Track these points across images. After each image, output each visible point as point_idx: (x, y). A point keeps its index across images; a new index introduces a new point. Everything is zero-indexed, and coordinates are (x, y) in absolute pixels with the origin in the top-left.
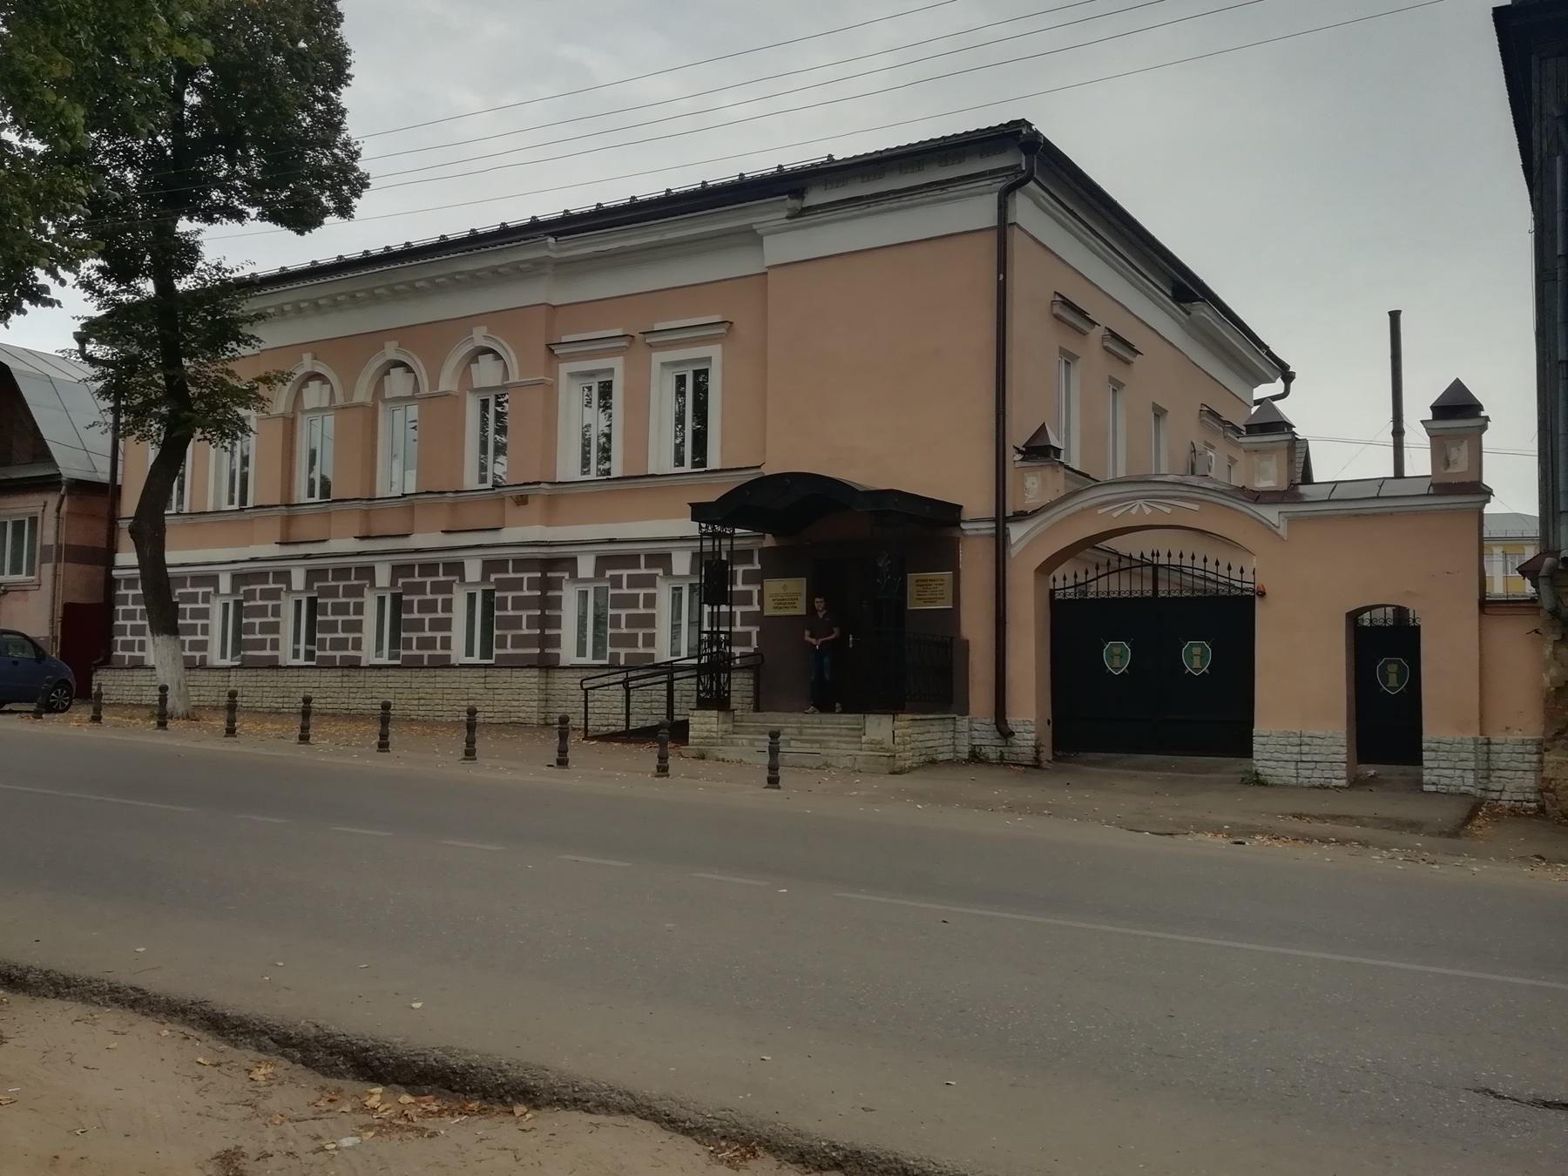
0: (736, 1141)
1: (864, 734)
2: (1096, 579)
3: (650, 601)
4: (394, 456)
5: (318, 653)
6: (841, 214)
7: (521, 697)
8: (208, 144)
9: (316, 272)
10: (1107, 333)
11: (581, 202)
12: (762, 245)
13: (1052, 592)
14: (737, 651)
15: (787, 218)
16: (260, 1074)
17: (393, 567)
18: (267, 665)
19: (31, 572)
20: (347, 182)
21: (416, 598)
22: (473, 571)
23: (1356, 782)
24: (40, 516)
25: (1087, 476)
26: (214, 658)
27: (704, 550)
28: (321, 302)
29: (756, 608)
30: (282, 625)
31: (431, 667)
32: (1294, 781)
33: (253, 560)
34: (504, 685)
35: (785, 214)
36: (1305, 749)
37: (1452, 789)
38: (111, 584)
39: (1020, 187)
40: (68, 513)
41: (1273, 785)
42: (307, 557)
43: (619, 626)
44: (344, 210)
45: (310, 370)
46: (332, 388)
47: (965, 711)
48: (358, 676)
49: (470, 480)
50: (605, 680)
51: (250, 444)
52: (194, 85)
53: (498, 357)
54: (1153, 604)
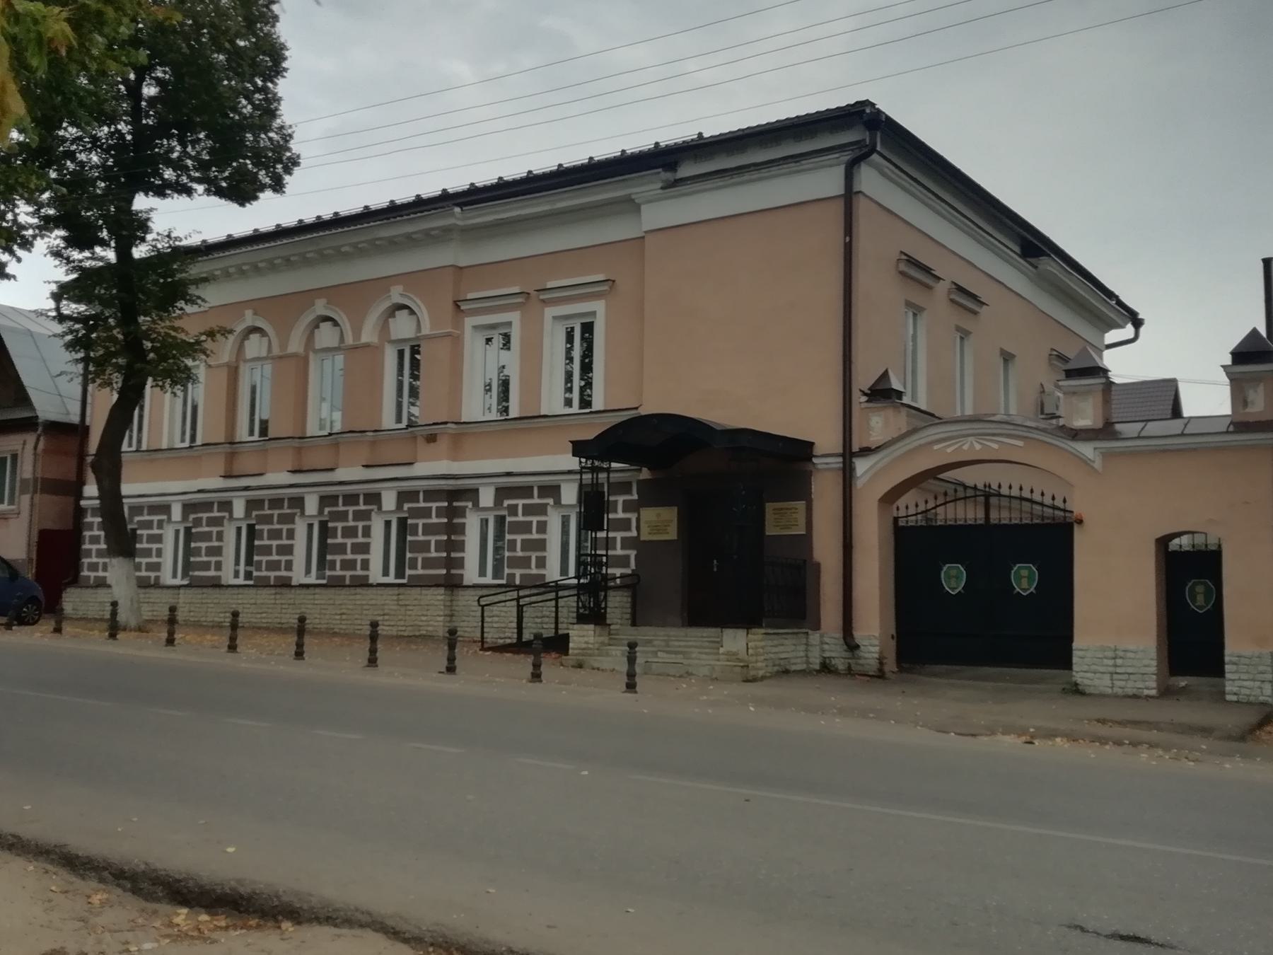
0: (440, 947)
1: (722, 646)
2: (945, 504)
3: (542, 527)
4: (323, 399)
5: (255, 574)
6: (708, 185)
7: (429, 613)
8: (162, 130)
9: (257, 238)
10: (954, 287)
11: (485, 176)
12: (640, 216)
13: (896, 519)
14: (617, 572)
15: (662, 188)
16: (96, 899)
17: (497, 489)
18: (358, 584)
19: (11, 502)
20: (281, 161)
21: (340, 525)
22: (389, 501)
23: (1166, 692)
24: (19, 452)
25: (932, 415)
26: (167, 578)
27: (584, 482)
28: (260, 265)
29: (634, 533)
30: (224, 550)
31: (353, 586)
32: (1109, 691)
33: (200, 491)
34: (416, 602)
35: (660, 185)
36: (1119, 662)
37: (1252, 699)
38: (80, 512)
39: (865, 159)
40: (45, 451)
41: (1090, 695)
42: (247, 488)
43: (514, 550)
44: (278, 186)
45: (251, 324)
46: (270, 341)
47: (817, 626)
48: (289, 595)
49: (388, 421)
50: (496, 599)
51: (198, 392)
52: (152, 78)
53: (412, 312)
54: (987, 530)
